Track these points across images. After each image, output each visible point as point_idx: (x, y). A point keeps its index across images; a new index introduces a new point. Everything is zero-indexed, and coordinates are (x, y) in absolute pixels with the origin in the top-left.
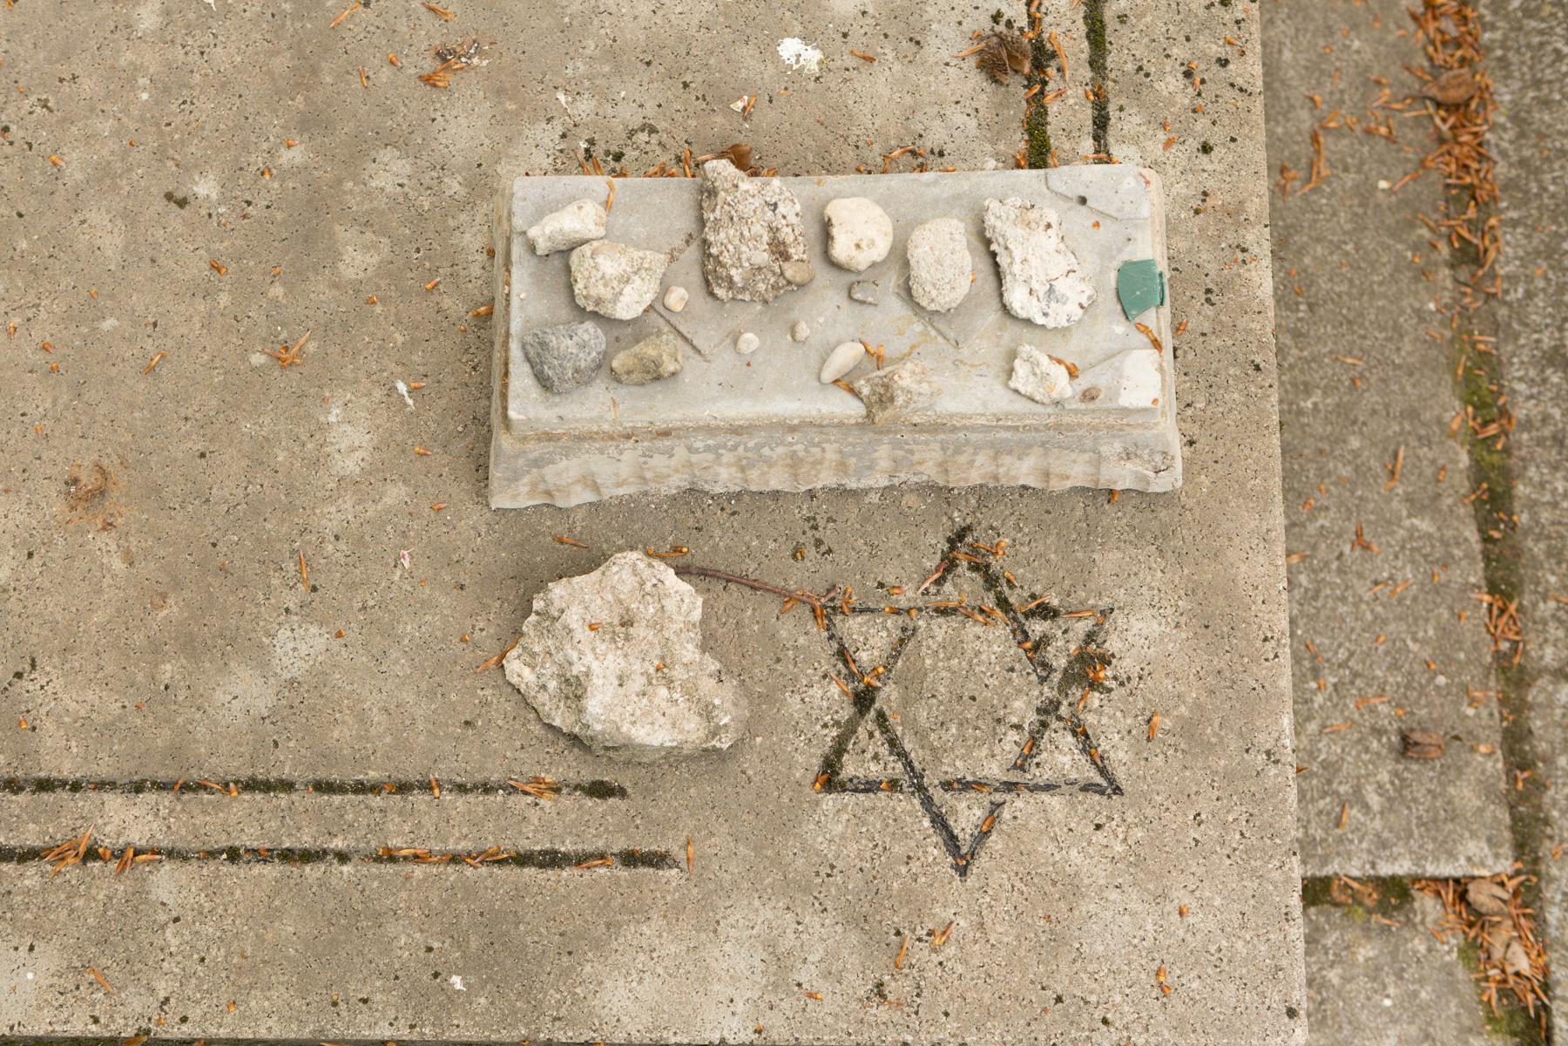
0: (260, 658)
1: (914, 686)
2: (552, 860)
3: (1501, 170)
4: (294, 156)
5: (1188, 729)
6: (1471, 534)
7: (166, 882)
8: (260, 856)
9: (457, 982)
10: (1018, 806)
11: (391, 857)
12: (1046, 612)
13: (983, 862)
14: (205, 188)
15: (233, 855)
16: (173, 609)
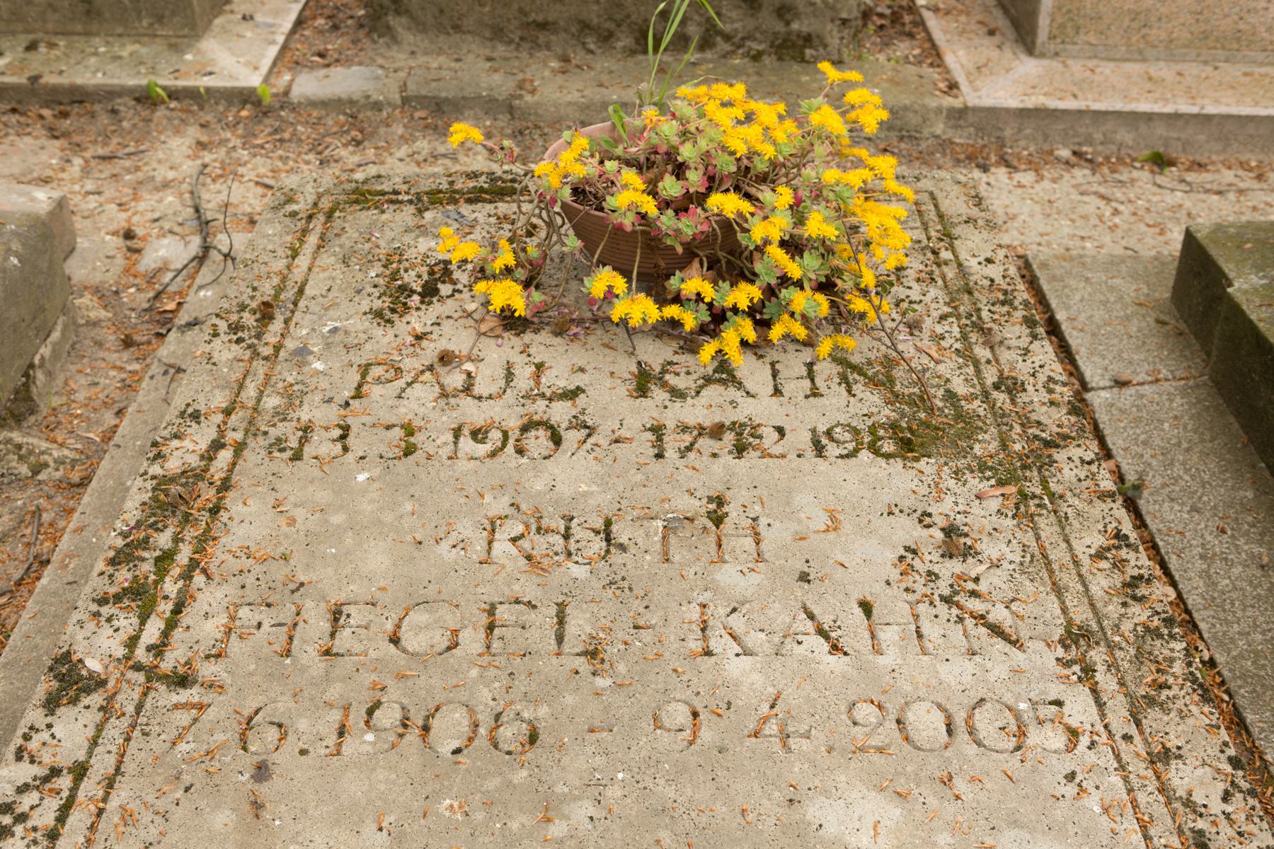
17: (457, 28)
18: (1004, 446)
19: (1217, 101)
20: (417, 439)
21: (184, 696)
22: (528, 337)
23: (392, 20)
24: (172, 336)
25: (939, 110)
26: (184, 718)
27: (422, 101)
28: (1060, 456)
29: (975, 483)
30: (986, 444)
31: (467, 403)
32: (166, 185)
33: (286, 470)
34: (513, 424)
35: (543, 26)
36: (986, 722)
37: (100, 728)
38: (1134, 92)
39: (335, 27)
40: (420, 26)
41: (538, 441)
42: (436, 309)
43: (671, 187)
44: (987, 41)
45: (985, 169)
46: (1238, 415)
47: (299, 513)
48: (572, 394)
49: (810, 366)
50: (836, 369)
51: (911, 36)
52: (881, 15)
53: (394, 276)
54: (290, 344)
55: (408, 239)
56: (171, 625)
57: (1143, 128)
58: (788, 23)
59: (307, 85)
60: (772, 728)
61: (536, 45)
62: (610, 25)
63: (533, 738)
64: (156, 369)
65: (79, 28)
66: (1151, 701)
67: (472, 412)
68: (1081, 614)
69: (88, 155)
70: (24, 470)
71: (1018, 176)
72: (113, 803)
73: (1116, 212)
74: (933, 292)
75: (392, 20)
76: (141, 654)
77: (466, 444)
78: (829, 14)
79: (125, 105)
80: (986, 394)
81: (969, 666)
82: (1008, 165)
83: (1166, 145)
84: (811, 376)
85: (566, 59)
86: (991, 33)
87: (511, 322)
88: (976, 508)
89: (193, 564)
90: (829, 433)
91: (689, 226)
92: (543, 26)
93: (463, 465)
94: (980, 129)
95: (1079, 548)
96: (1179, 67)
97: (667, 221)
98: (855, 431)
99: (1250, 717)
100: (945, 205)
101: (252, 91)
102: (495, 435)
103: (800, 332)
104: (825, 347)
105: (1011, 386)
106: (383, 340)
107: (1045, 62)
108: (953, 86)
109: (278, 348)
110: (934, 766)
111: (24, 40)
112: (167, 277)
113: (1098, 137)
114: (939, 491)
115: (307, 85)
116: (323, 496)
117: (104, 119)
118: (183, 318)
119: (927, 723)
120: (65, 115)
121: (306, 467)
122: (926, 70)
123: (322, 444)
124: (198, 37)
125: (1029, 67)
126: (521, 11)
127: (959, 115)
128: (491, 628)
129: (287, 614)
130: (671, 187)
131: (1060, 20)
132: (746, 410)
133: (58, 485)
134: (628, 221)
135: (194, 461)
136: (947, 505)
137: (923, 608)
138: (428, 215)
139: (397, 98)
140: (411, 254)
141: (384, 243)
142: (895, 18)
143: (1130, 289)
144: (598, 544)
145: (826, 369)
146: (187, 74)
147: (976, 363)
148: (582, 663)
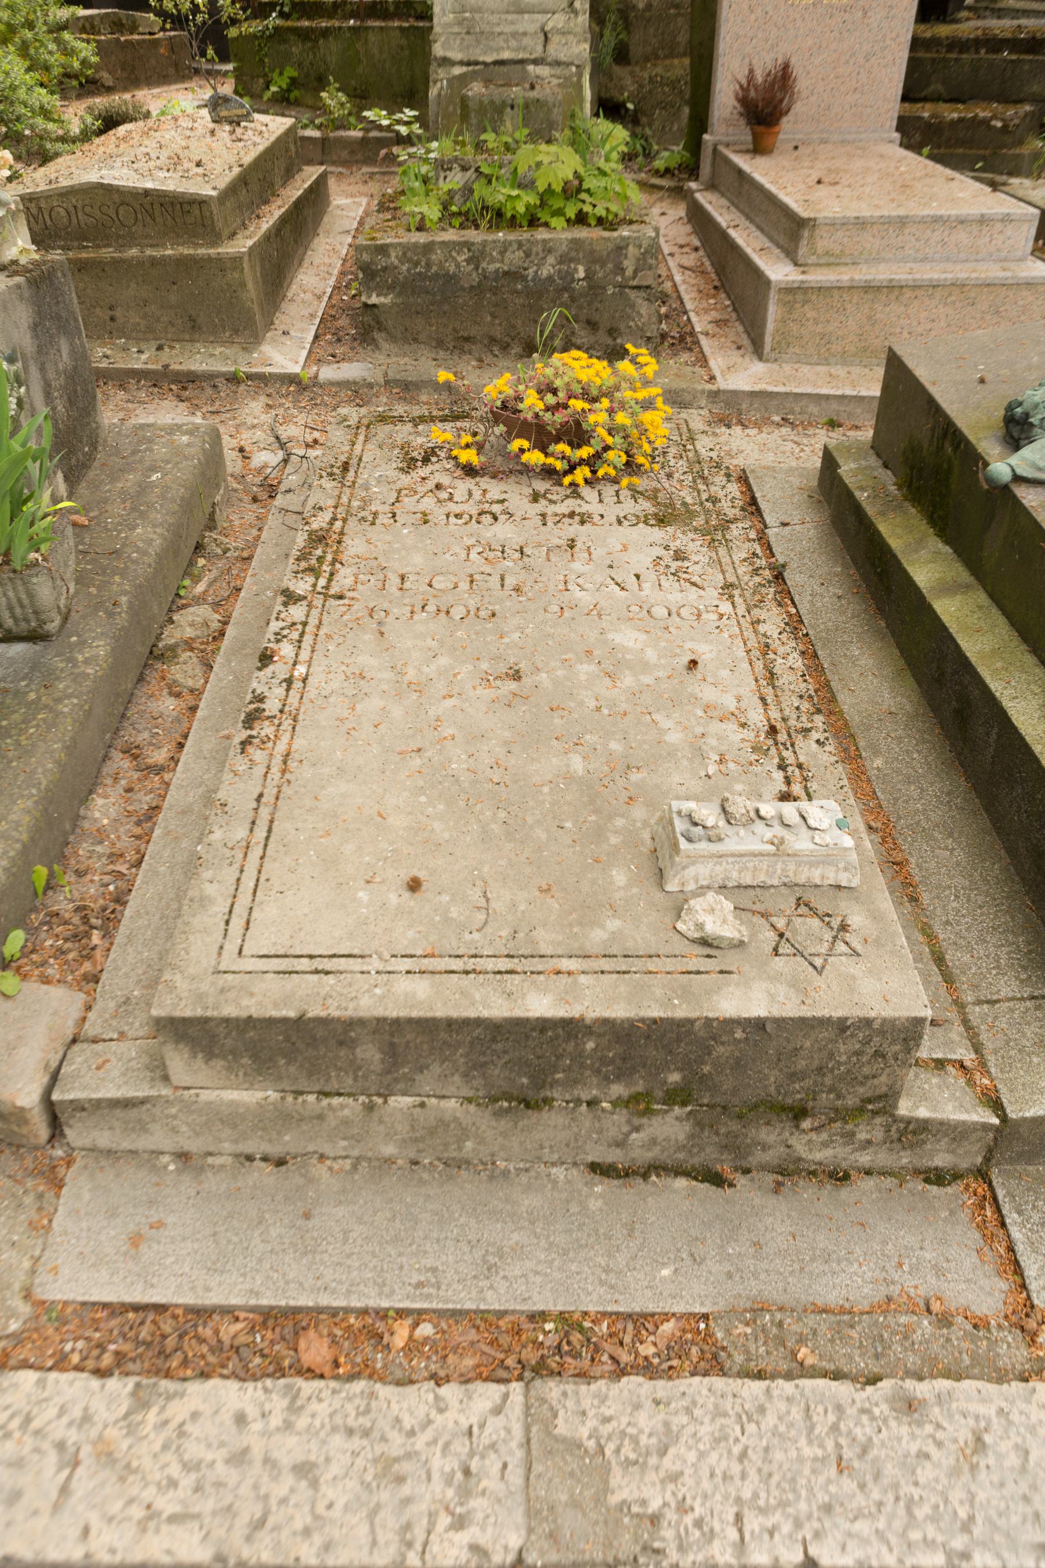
0: (603, 927)
1: (795, 932)
2: (698, 972)
3: (917, 878)
4: (593, 818)
5: (877, 941)
6: (935, 968)
7: (582, 979)
8: (610, 972)
9: (676, 1002)
10: (831, 959)
11: (650, 972)
12: (828, 915)
13: (825, 972)
14: (568, 825)
15: (602, 972)
16: (574, 916)
17: (415, 340)
18: (707, 522)
19: (869, 389)
20: (429, 517)
21: (341, 602)
22: (478, 479)
23: (376, 335)
24: (279, 496)
25: (703, 392)
26: (345, 609)
27: (397, 382)
28: (733, 526)
29: (691, 535)
30: (699, 521)
31: (451, 505)
32: (254, 427)
33: (370, 529)
34: (474, 512)
35: (467, 339)
36: (684, 612)
37: (309, 612)
38: (820, 383)
39: (339, 340)
40: (393, 338)
41: (487, 519)
42: (430, 468)
43: (550, 399)
44: (736, 353)
45: (729, 426)
46: (840, 536)
47: (379, 544)
48: (502, 501)
49: (617, 492)
50: (629, 493)
51: (690, 350)
52: (673, 337)
53: (407, 453)
54: (360, 481)
55: (411, 438)
56: (330, 580)
57: (824, 404)
58: (615, 339)
59: (328, 373)
60: (595, 612)
61: (463, 352)
62: (506, 339)
63: (494, 615)
64: (273, 510)
65: (187, 337)
66: (756, 606)
67: (456, 509)
68: (731, 579)
69: (204, 410)
70: (219, 551)
71: (747, 431)
72: (321, 633)
73: (802, 450)
74: (681, 462)
75: (376, 335)
76: (319, 589)
77: (452, 519)
78: (639, 333)
79: (221, 382)
80: (701, 504)
81: (680, 595)
82: (743, 425)
83: (838, 415)
84: (617, 496)
85: (481, 360)
86: (739, 348)
87: (470, 471)
88: (691, 544)
89: (334, 561)
90: (625, 517)
91: (559, 417)
92: (467, 339)
93: (452, 527)
94: (727, 404)
95: (735, 558)
96: (848, 369)
97: (548, 416)
98: (637, 516)
99: (819, 653)
100: (692, 425)
101: (297, 375)
102: (466, 517)
103: (613, 472)
104: (625, 482)
105: (714, 500)
106: (405, 480)
107: (769, 365)
108: (712, 378)
109: (354, 483)
110: (662, 624)
111: (154, 344)
112: (269, 470)
113: (798, 409)
114: (674, 538)
115: (328, 373)
116: (389, 538)
117: (209, 391)
118: (283, 488)
119: (660, 612)
120: (184, 388)
121: (378, 527)
122: (697, 369)
123: (383, 519)
124: (259, 343)
125: (759, 368)
126: (454, 329)
127: (715, 395)
128: (472, 582)
129: (381, 577)
130: (550, 399)
131: (778, 338)
132: (585, 508)
133: (237, 559)
134: (529, 416)
135: (324, 525)
136: (678, 543)
137: (662, 577)
138: (420, 427)
139: (382, 381)
140: (414, 444)
141: (399, 440)
142: (682, 339)
143: (796, 481)
144: (518, 555)
145: (625, 494)
146: (256, 365)
147: (699, 492)
148: (513, 593)
